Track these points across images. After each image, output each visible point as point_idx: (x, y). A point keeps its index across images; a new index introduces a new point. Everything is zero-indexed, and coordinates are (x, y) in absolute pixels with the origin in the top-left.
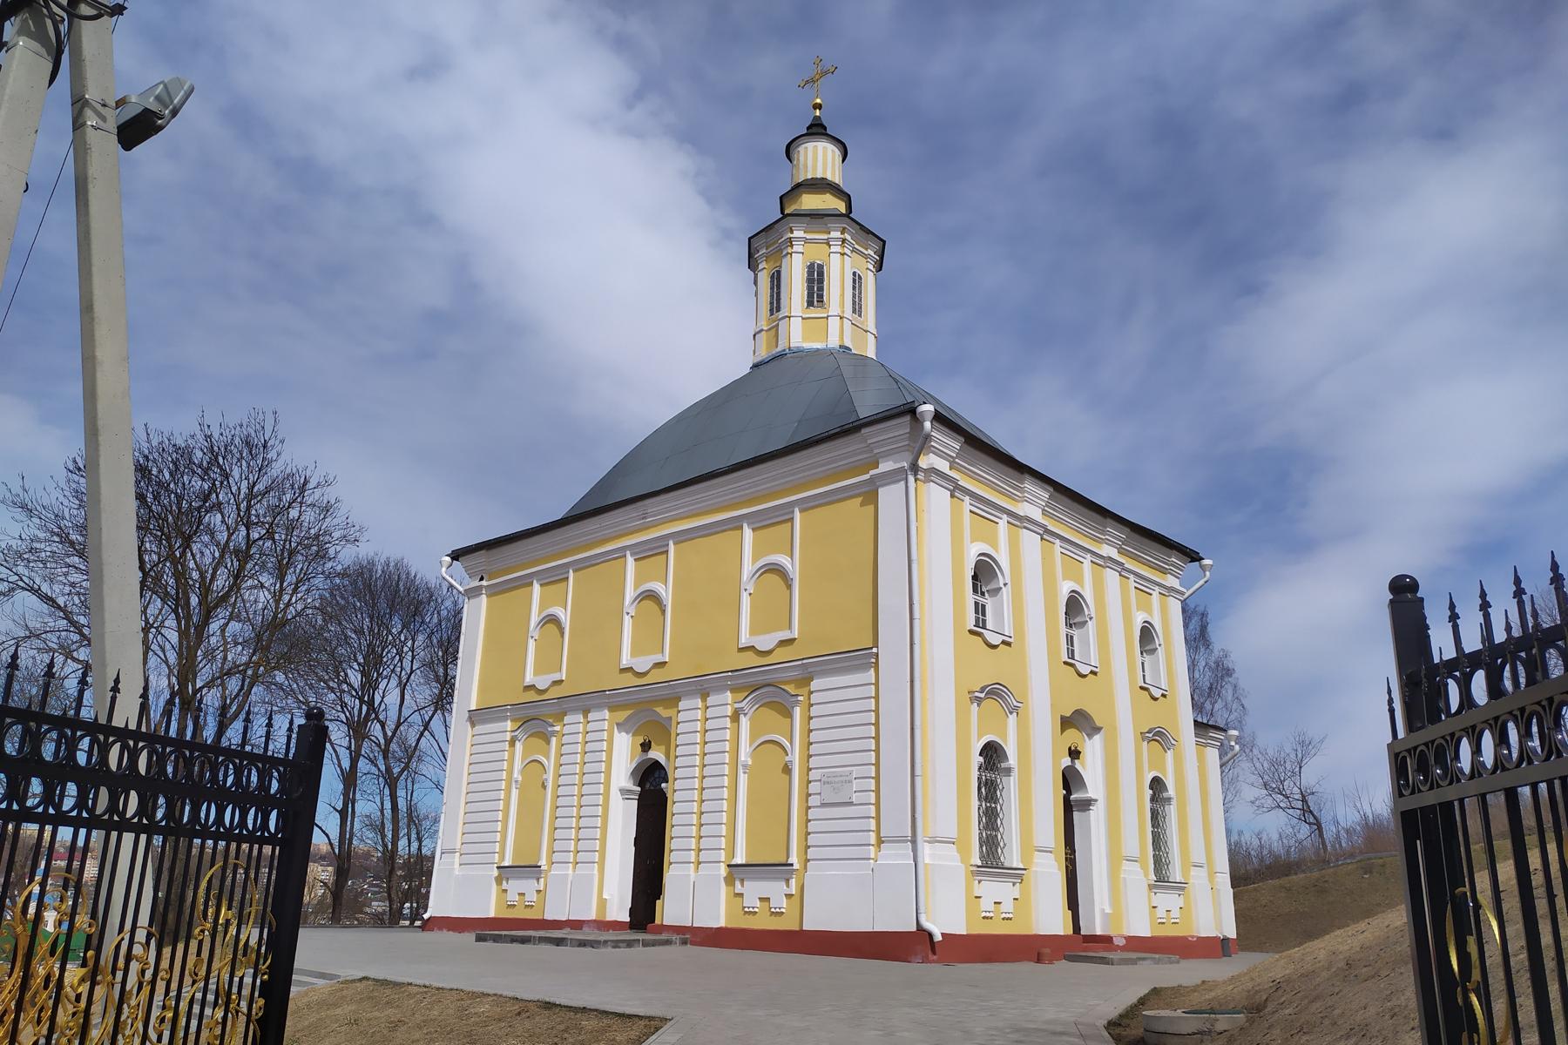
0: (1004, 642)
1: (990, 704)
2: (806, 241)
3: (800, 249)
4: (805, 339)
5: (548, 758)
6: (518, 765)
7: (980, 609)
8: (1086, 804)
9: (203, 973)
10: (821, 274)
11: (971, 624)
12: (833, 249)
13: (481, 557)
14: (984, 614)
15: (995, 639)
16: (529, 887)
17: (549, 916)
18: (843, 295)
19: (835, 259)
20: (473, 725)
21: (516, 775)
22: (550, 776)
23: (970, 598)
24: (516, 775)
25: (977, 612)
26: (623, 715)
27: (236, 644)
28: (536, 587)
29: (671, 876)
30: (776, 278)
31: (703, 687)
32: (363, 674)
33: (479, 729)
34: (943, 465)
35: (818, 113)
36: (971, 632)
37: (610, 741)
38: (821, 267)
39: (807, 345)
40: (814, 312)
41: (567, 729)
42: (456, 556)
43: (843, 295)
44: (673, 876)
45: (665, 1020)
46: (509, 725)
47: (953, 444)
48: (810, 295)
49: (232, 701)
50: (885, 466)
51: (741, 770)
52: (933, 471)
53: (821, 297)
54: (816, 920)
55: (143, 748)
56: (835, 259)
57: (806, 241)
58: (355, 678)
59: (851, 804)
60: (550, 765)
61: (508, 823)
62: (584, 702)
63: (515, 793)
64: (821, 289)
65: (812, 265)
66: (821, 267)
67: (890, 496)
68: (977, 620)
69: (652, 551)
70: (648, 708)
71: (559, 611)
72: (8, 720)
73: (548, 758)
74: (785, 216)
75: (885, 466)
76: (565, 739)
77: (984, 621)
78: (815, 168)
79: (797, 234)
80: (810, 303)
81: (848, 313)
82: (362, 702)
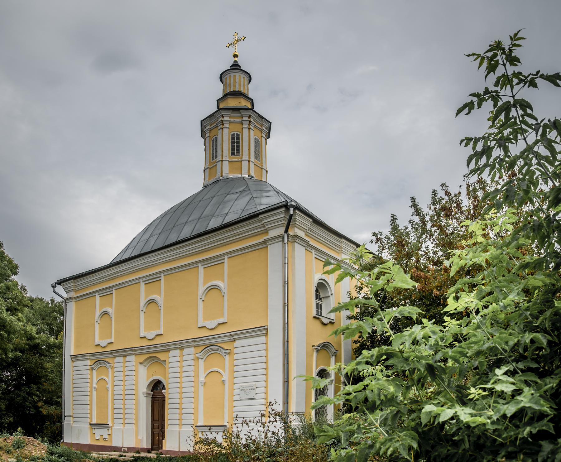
0: (330, 322)
1: (323, 353)
2: (231, 122)
3: (227, 126)
4: (230, 172)
5: (108, 377)
6: (95, 381)
7: (319, 307)
10: (238, 139)
11: (314, 313)
12: (244, 126)
13: (71, 284)
14: (321, 309)
15: (326, 321)
16: (105, 433)
17: (114, 445)
19: (246, 131)
20: (73, 361)
21: (95, 385)
22: (110, 386)
23: (314, 302)
24: (95, 385)
25: (317, 308)
26: (143, 358)
28: (98, 297)
29: (168, 429)
30: (215, 142)
31: (180, 345)
33: (76, 363)
34: (301, 234)
35: (236, 59)
36: (314, 317)
37: (137, 371)
38: (238, 135)
39: (231, 176)
40: (235, 158)
41: (116, 365)
43: (249, 149)
44: (170, 429)
46: (89, 362)
47: (308, 222)
50: (273, 233)
51: (93, 390)
52: (296, 236)
53: (238, 150)
56: (246, 131)
57: (231, 122)
59: (255, 399)
60: (109, 380)
61: (100, 404)
62: (124, 352)
63: (94, 393)
65: (233, 135)
66: (238, 135)
67: (275, 250)
68: (317, 311)
69: (152, 280)
70: (153, 354)
71: (109, 310)
73: (108, 377)
74: (219, 109)
75: (273, 233)
76: (116, 370)
77: (321, 313)
78: (235, 86)
79: (226, 118)
80: (233, 154)
81: (252, 159)
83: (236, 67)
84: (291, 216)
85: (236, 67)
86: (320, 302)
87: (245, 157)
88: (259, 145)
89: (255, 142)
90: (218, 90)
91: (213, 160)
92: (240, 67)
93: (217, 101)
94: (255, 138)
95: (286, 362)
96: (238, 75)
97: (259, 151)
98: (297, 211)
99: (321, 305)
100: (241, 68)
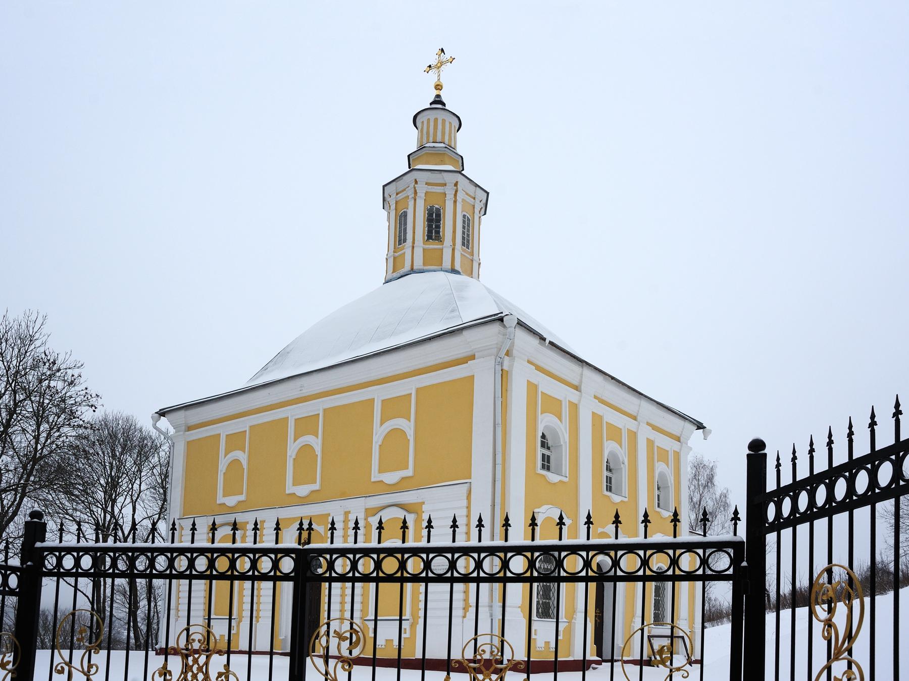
8: (643, 522)
9: (348, 615)
10: (438, 215)
18: (454, 232)
27: (8, 471)
32: (105, 492)
38: (438, 210)
42: (162, 413)
43: (454, 232)
45: (580, 391)
48: (430, 232)
49: (9, 508)
53: (438, 232)
54: (893, 558)
55: (109, 569)
58: (100, 495)
64: (438, 227)
65: (432, 207)
66: (438, 210)
72: (92, 571)
80: (430, 237)
82: (105, 512)
83: (438, 101)
84: (658, 619)
85: (438, 101)
86: (547, 452)
87: (421, 204)
88: (468, 226)
89: (464, 222)
90: (410, 140)
91: (400, 244)
92: (444, 104)
93: (409, 156)
94: (464, 216)
95: (499, 468)
96: (440, 115)
97: (468, 235)
98: (771, 486)
99: (549, 457)
100: (447, 108)
